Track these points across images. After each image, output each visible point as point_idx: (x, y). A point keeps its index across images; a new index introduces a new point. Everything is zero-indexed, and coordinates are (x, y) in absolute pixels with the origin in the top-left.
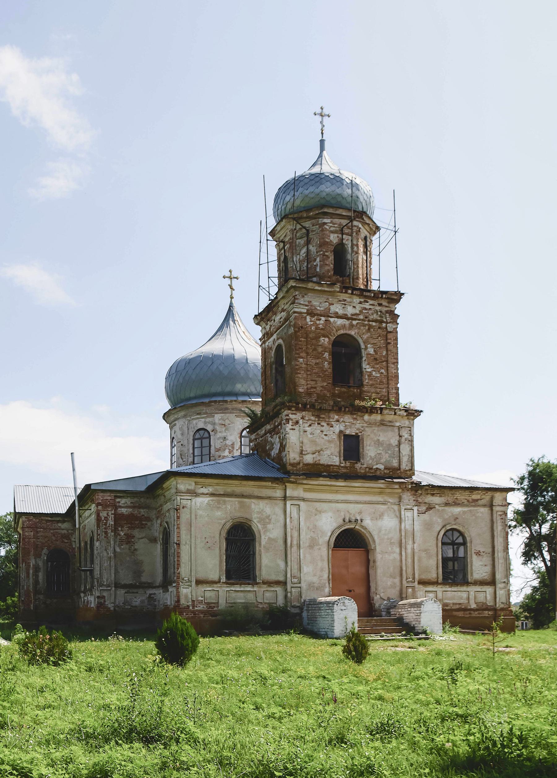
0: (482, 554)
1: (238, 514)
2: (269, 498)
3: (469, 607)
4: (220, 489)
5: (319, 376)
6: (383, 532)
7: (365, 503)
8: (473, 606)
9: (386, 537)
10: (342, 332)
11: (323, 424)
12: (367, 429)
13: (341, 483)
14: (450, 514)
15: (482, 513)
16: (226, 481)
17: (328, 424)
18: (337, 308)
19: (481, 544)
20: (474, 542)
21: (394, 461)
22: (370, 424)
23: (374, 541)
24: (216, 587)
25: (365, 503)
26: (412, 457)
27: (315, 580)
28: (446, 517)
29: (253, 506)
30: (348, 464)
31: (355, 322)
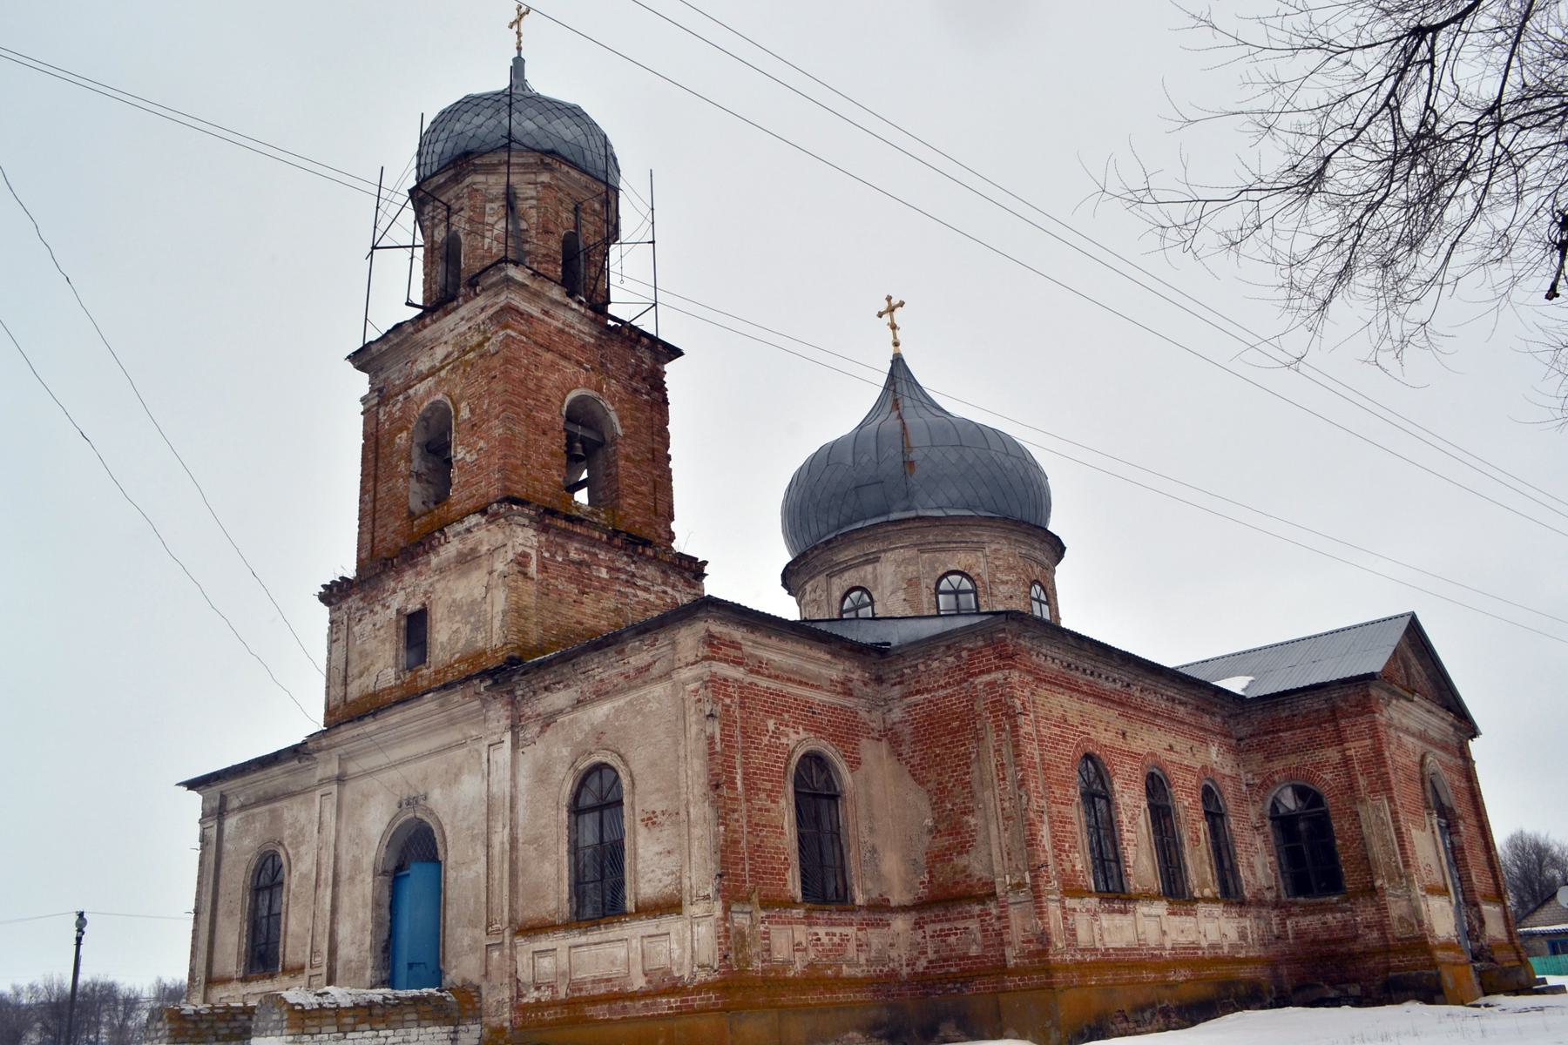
7: (431, 753)
8: (639, 983)
15: (659, 700)
18: (423, 365)
19: (658, 790)
20: (640, 787)
25: (431, 753)
31: (443, 373)
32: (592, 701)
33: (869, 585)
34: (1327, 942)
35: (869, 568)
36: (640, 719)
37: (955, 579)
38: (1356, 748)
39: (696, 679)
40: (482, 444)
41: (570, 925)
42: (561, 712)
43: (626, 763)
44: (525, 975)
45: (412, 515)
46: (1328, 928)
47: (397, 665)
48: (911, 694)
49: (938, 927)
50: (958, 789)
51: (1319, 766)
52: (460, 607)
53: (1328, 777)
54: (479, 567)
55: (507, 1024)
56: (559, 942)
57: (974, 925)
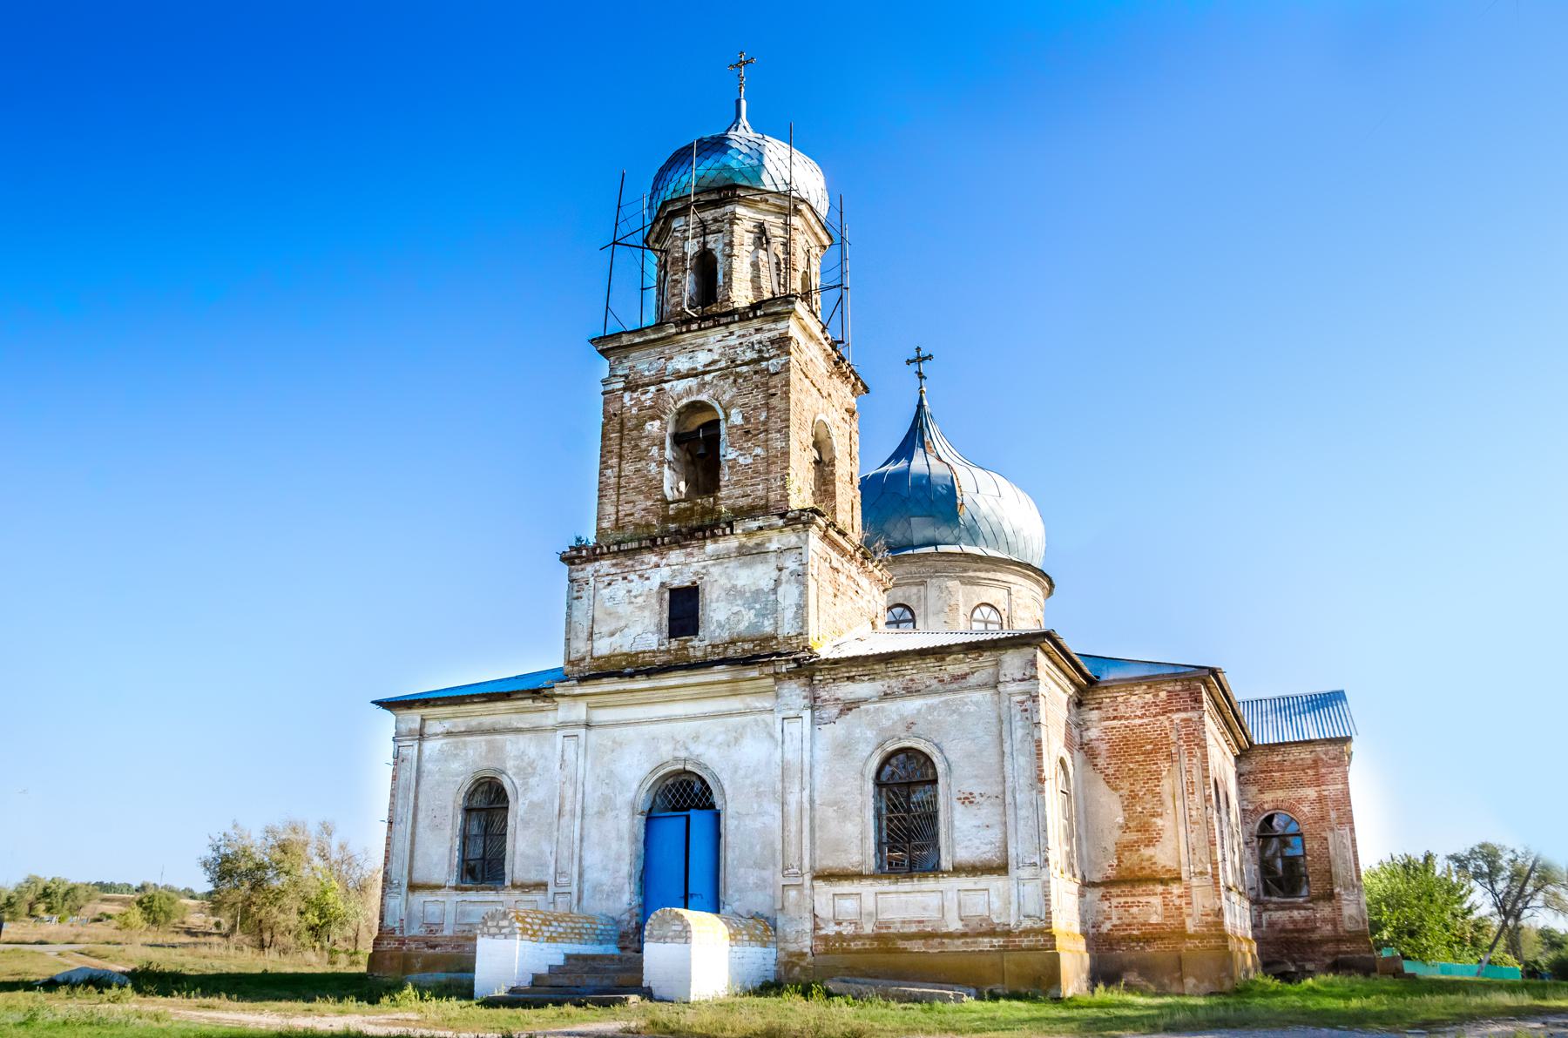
0: (978, 799)
1: (485, 764)
2: (534, 729)
3: (944, 930)
4: (460, 724)
5: (641, 492)
6: (741, 772)
7: (705, 716)
8: (955, 925)
9: (748, 782)
10: (685, 401)
11: (632, 576)
12: (712, 570)
13: (641, 683)
14: (895, 717)
15: (976, 704)
16: (463, 708)
17: (641, 576)
18: (682, 363)
20: (956, 772)
21: (766, 623)
22: (718, 558)
23: (723, 793)
24: (439, 896)
25: (705, 716)
26: (802, 608)
27: (605, 878)
28: (886, 723)
29: (509, 747)
30: (674, 644)
31: (708, 378)
32: (902, 696)
33: (912, 604)
34: (1292, 931)
35: (914, 589)
36: (955, 717)
37: (986, 610)
38: (1332, 790)
39: (1023, 693)
40: (758, 451)
41: (873, 876)
42: (866, 700)
43: (941, 751)
44: (824, 911)
45: (665, 501)
46: (1294, 922)
47: (660, 631)
48: (1108, 719)
49: (1122, 900)
50: (1149, 797)
51: (1299, 801)
52: (741, 593)
53: (1306, 809)
54: (765, 561)
55: (807, 950)
56: (867, 889)
57: (1156, 901)
